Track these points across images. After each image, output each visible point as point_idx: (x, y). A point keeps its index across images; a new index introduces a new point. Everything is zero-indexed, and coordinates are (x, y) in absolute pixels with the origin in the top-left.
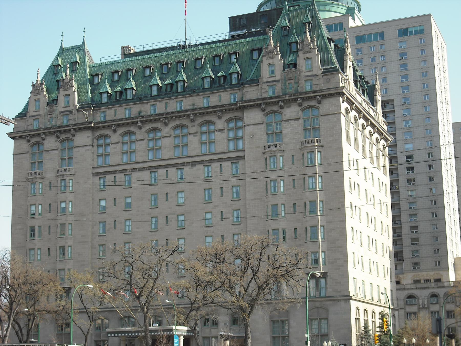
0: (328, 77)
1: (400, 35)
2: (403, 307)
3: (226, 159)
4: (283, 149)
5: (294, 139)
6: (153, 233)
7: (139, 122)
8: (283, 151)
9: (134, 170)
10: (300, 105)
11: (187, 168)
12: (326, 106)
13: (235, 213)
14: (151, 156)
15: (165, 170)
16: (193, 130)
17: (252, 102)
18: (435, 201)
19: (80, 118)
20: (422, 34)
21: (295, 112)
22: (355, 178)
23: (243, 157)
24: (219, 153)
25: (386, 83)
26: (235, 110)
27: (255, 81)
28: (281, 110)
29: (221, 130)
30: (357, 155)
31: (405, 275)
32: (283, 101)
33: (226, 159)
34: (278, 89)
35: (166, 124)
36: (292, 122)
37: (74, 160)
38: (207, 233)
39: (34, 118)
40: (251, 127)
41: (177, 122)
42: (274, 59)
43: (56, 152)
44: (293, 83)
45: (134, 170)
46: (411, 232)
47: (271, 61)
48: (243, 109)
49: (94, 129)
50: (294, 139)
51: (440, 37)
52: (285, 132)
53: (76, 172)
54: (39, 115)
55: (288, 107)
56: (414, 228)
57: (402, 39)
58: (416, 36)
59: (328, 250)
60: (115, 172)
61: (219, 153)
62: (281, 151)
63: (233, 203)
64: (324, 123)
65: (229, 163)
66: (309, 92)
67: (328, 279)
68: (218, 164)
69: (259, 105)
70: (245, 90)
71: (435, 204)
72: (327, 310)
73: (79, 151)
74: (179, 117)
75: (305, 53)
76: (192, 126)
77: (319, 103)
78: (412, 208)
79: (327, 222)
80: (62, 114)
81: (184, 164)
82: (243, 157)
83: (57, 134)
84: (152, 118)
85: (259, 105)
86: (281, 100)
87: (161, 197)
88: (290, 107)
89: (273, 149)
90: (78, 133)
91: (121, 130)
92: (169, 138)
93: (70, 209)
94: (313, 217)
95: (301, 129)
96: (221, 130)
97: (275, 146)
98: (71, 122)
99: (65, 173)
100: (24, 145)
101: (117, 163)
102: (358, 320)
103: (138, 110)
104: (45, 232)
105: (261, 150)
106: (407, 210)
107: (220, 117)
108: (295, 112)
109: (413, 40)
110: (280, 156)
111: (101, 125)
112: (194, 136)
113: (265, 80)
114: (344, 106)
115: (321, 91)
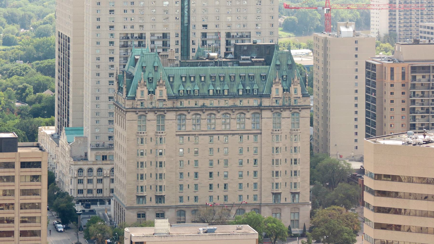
0: (305, 99)
3: (251, 134)
9: (200, 135)
11: (229, 136)
14: (223, 127)
15: (218, 136)
16: (233, 117)
19: (169, 104)
24: (247, 130)
27: (268, 96)
28: (300, 112)
32: (283, 109)
33: (251, 134)
34: (280, 102)
35: (219, 112)
36: (286, 119)
37: (166, 127)
41: (225, 112)
43: (154, 121)
45: (200, 135)
52: (283, 123)
53: (167, 134)
54: (144, 100)
55: (284, 111)
59: (301, 182)
60: (189, 135)
61: (247, 130)
65: (252, 136)
67: (300, 195)
69: (271, 109)
70: (263, 100)
72: (299, 209)
73: (168, 122)
74: (226, 110)
75: (294, 85)
76: (233, 115)
77: (300, 111)
79: (301, 169)
81: (228, 134)
83: (156, 112)
84: (212, 109)
85: (271, 109)
87: (216, 150)
88: (286, 111)
89: (142, 134)
90: (168, 112)
91: (192, 113)
92: (220, 120)
95: (290, 123)
97: (143, 133)
98: (165, 106)
99: (162, 134)
101: (190, 130)
103: (203, 103)
104: (148, 165)
105: (271, 131)
107: (248, 112)
113: (274, 96)
115: (302, 106)
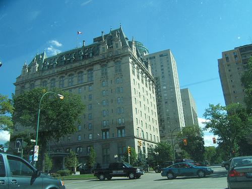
3: (87, 85)
10: (114, 61)
12: (124, 59)
13: (90, 125)
22: (140, 119)
23: (93, 83)
26: (90, 66)
27: (98, 55)
29: (85, 74)
30: (136, 80)
33: (87, 85)
48: (93, 65)
49: (41, 79)
51: (174, 59)
64: (123, 66)
68: (84, 87)
93: (37, 70)
95: (114, 70)
96: (85, 74)
100: (19, 87)
102: (139, 147)
114: (131, 60)
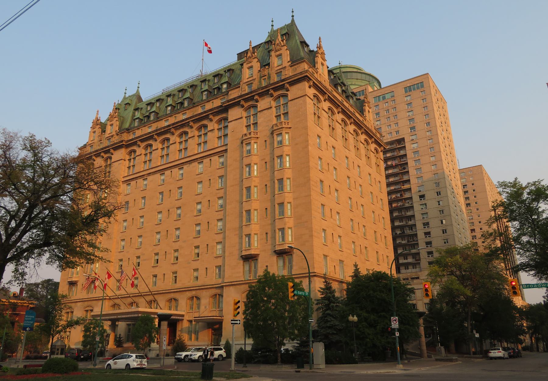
1: (406, 92)
2: (421, 299)
4: (257, 136)
5: (267, 126)
6: (158, 226)
7: (154, 135)
8: (258, 138)
11: (185, 167)
17: (233, 101)
18: (443, 211)
20: (422, 89)
21: (268, 102)
25: (398, 127)
31: (422, 272)
36: (266, 111)
38: (197, 221)
39: (90, 145)
40: (233, 122)
42: (252, 63)
44: (267, 79)
46: (425, 237)
47: (250, 65)
49: (127, 146)
50: (267, 126)
56: (427, 234)
57: (408, 94)
58: (419, 90)
59: (295, 226)
62: (255, 138)
63: (218, 191)
66: (278, 82)
71: (443, 213)
78: (424, 218)
79: (294, 199)
80: (107, 139)
82: (226, 151)
86: (256, 94)
88: (264, 99)
94: (279, 195)
106: (420, 220)
108: (268, 102)
109: (416, 94)
110: (255, 142)
111: (130, 142)
112: (192, 139)
